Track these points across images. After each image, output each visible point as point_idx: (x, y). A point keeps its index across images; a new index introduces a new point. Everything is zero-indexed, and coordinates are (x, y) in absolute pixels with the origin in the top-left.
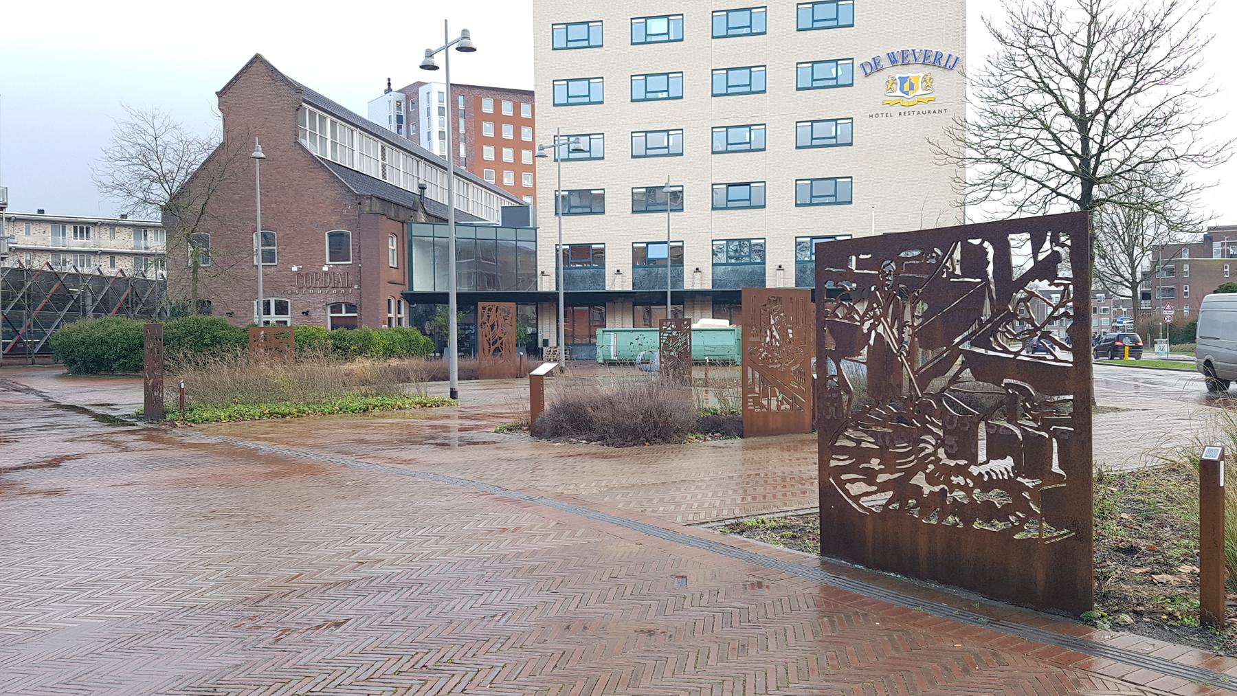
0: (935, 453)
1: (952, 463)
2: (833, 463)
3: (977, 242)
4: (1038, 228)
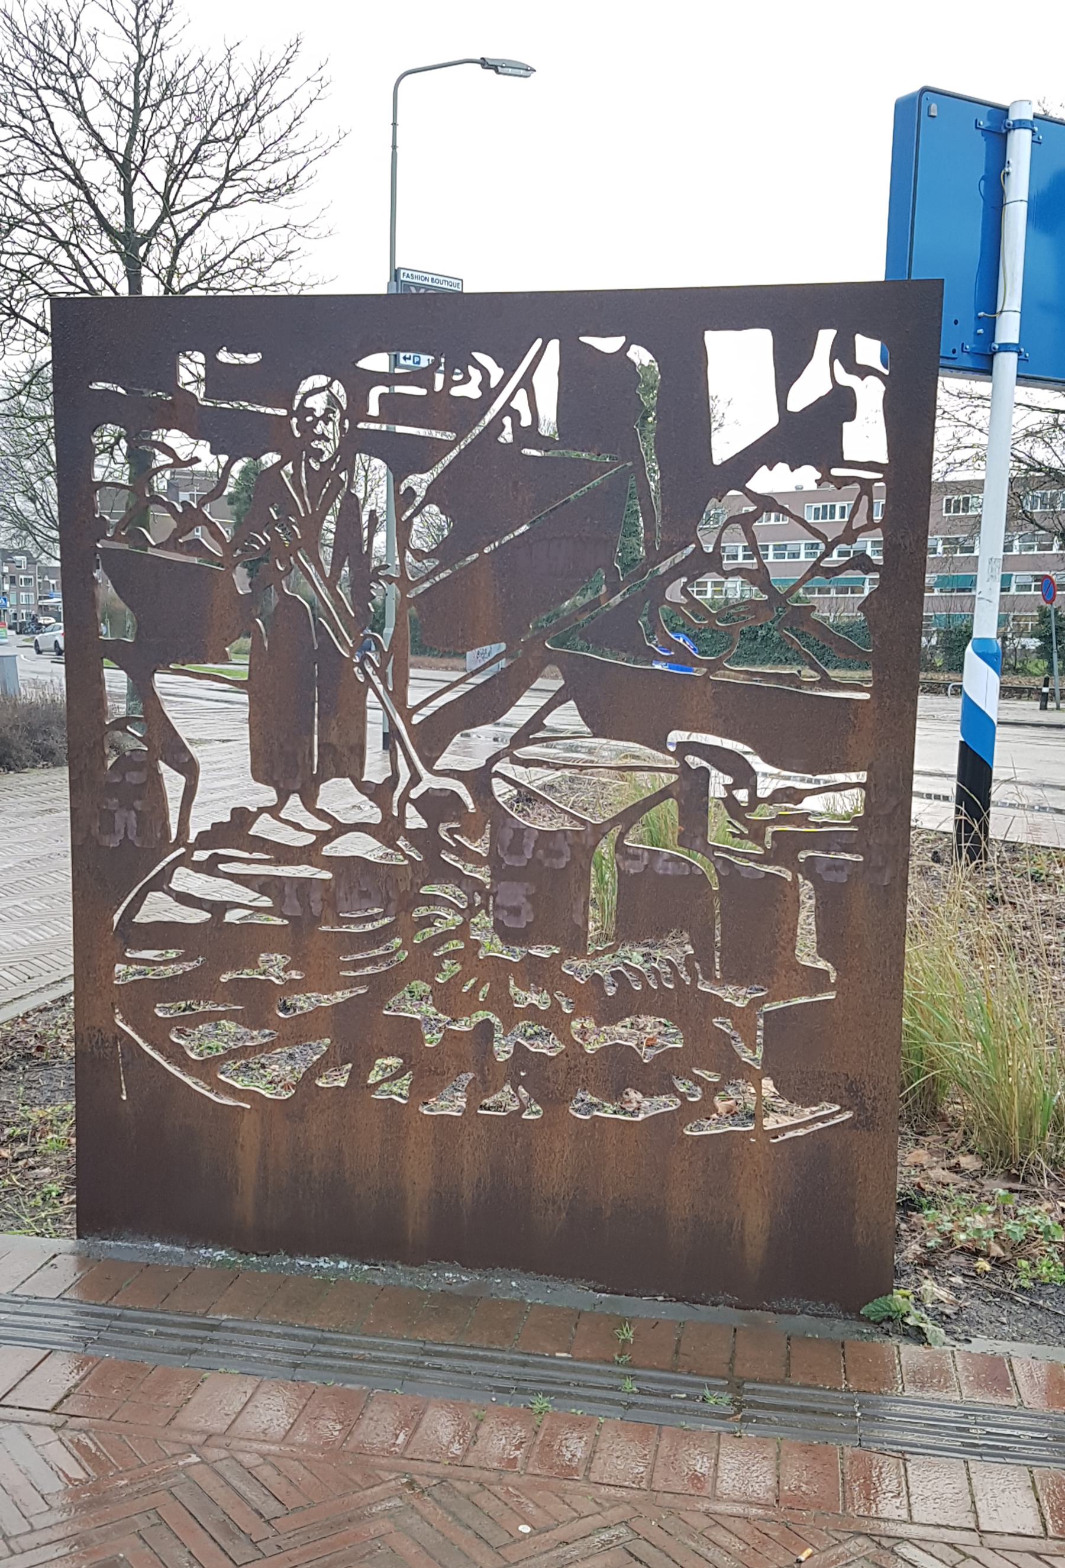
1: (514, 955)
3: (609, 345)
4: (791, 315)
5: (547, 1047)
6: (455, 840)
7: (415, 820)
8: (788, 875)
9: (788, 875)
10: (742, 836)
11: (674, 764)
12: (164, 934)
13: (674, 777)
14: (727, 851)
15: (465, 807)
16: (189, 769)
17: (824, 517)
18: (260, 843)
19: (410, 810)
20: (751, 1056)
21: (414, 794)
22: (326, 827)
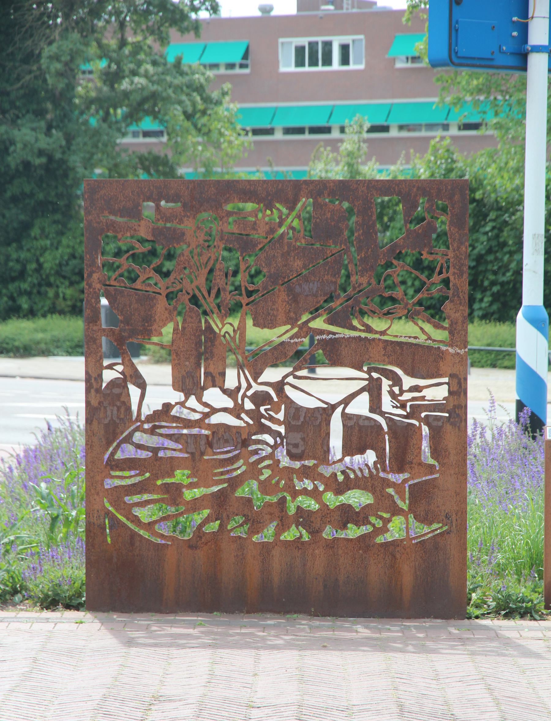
0: (271, 456)
1: (297, 465)
2: (109, 483)
5: (312, 505)
6: (268, 414)
7: (249, 405)
8: (416, 423)
9: (416, 423)
10: (397, 407)
11: (367, 376)
12: (130, 464)
13: (367, 382)
14: (391, 414)
15: (272, 398)
16: (142, 385)
17: (314, 62)
18: (177, 419)
19: (246, 400)
20: (404, 506)
21: (249, 393)
22: (207, 410)
